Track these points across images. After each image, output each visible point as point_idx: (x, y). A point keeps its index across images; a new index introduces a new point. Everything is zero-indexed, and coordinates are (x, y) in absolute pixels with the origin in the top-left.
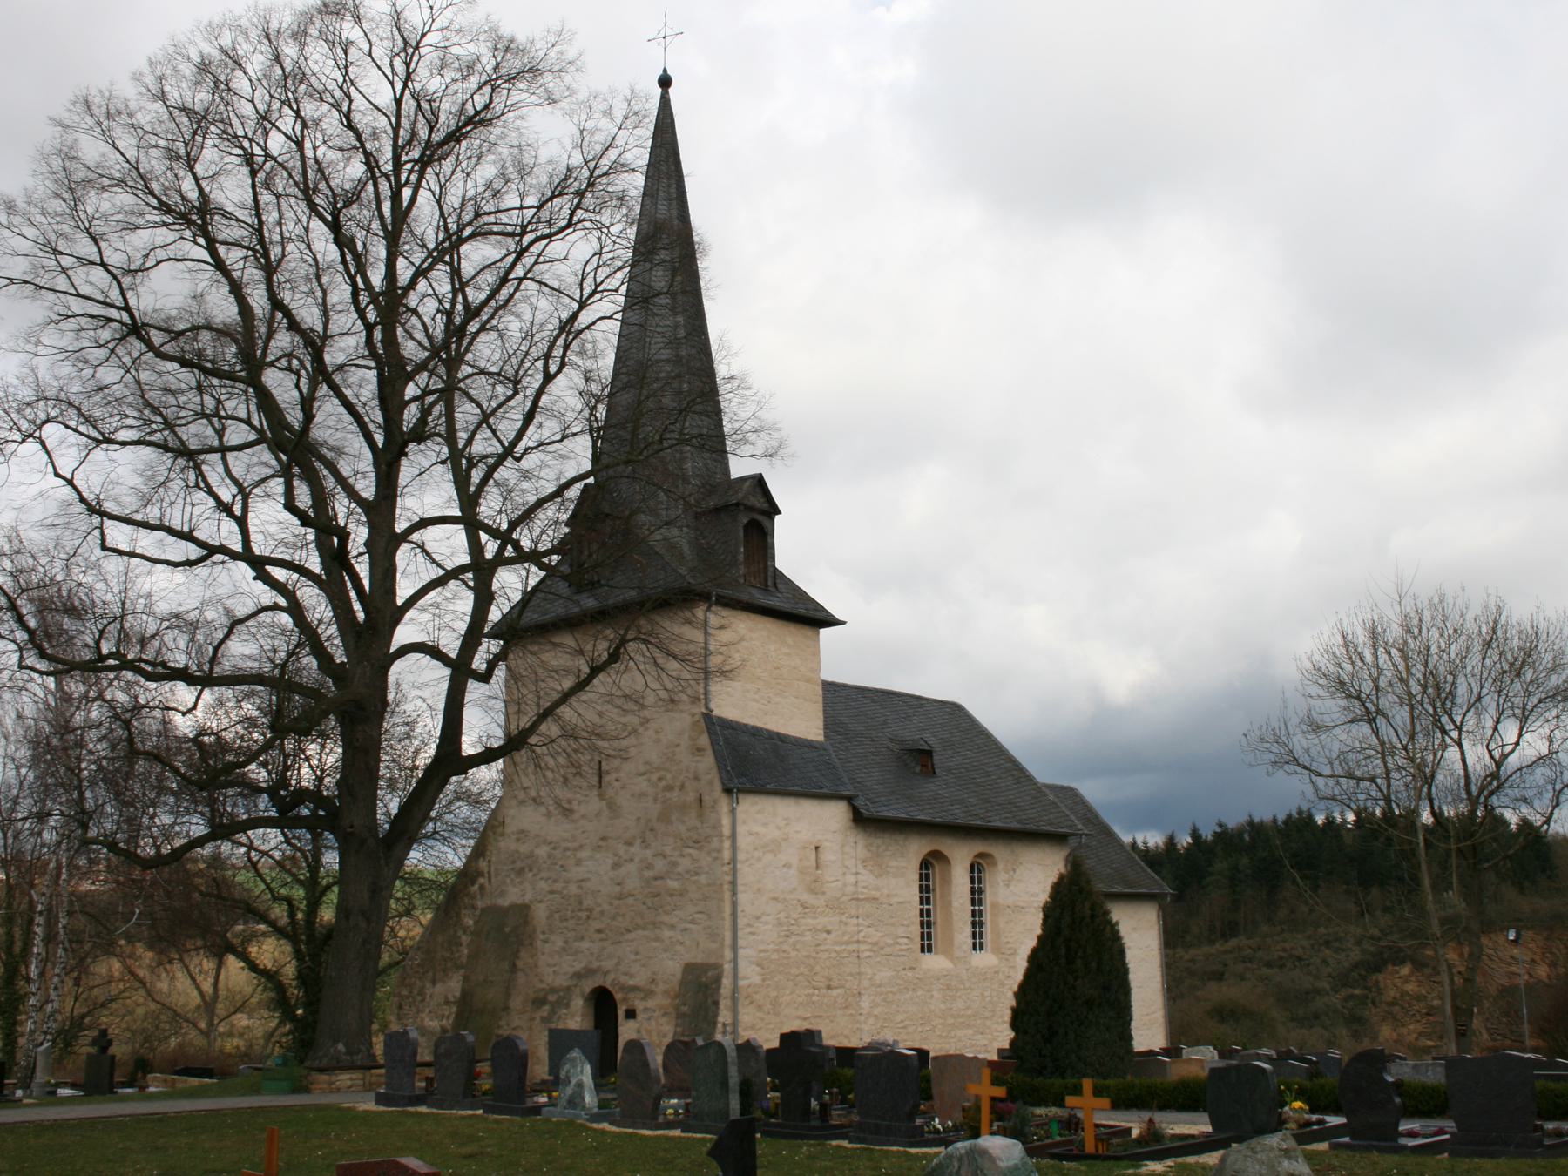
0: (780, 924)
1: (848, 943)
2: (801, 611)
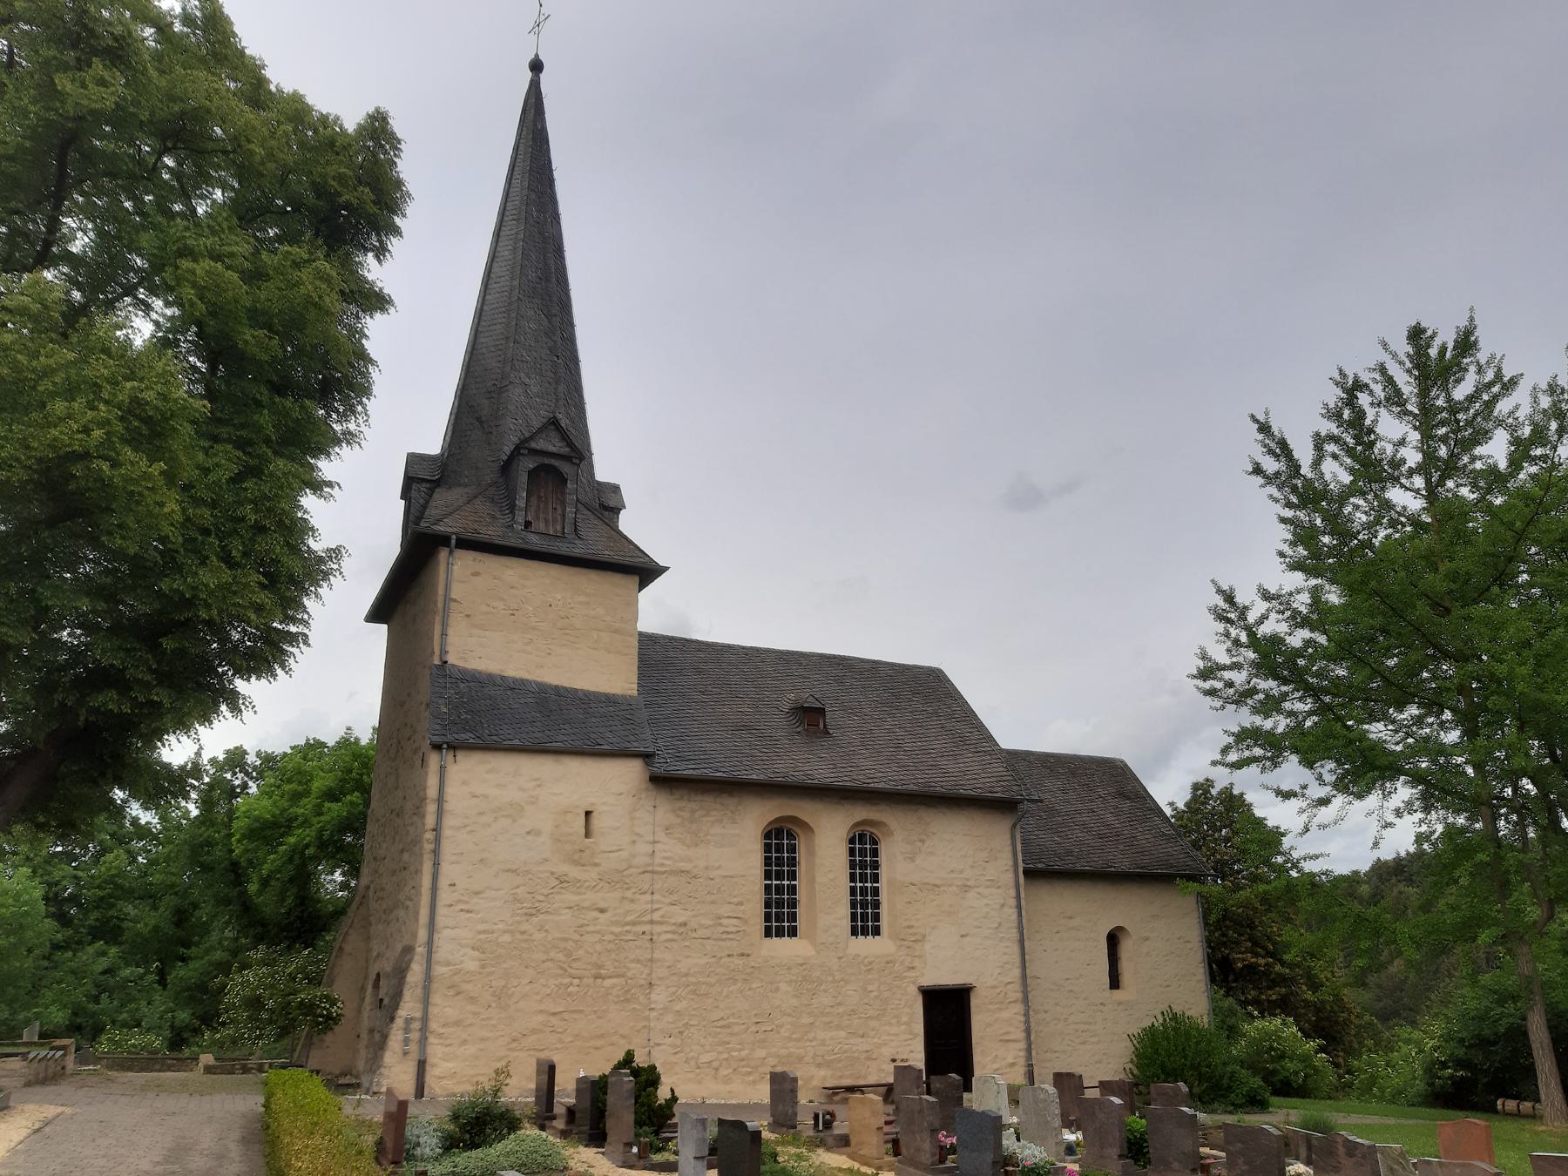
1: (634, 924)
2: (627, 560)
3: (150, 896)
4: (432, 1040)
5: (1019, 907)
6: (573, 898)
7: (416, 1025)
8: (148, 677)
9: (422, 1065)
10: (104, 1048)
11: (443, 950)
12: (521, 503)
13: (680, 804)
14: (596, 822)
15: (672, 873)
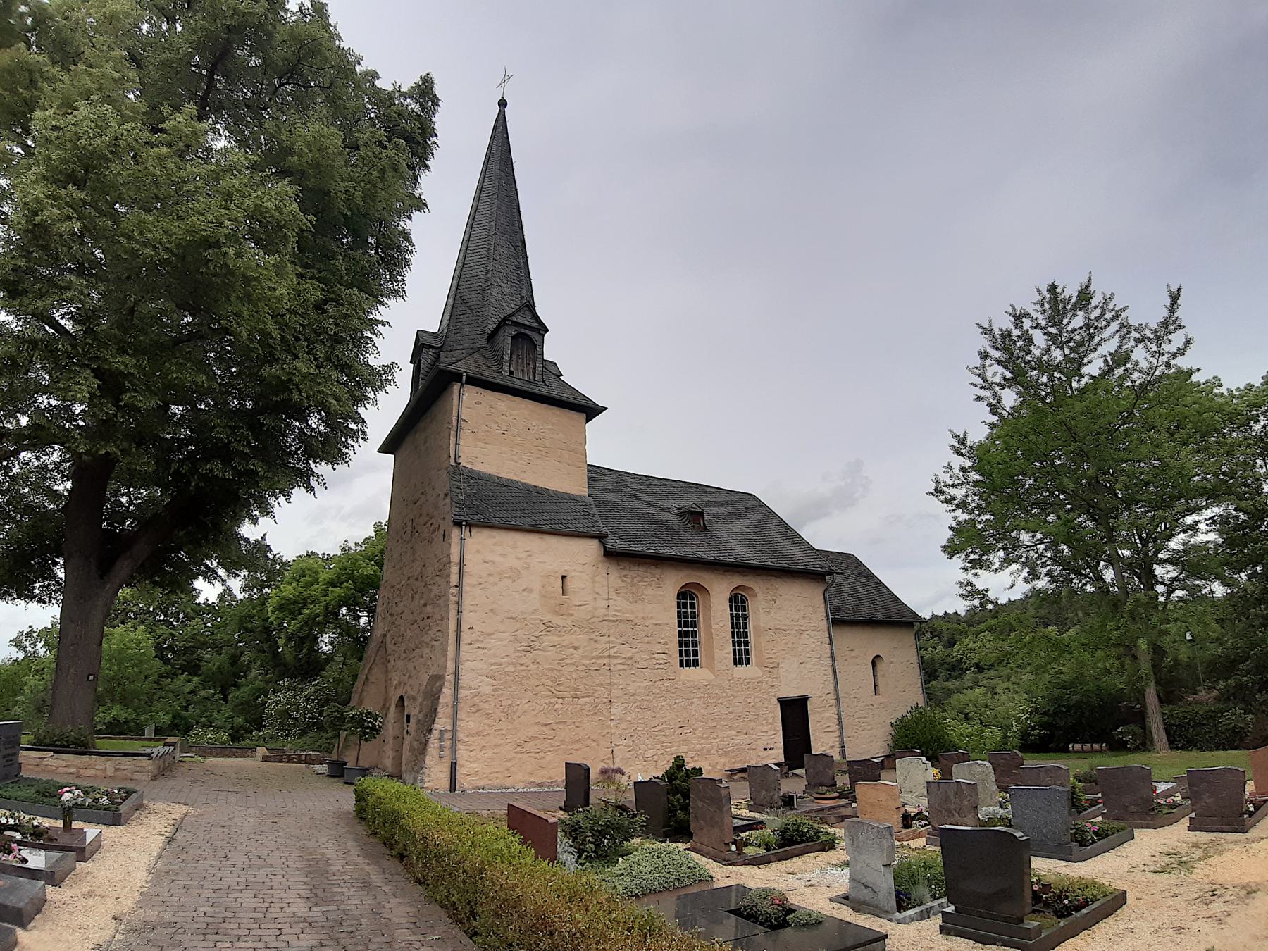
1: (597, 658)
3: (217, 648)
4: (460, 746)
5: (831, 643)
6: (556, 639)
7: (448, 735)
8: (247, 450)
9: (454, 766)
10: (193, 739)
11: (467, 678)
12: (507, 358)
13: (626, 572)
14: (570, 583)
15: (620, 621)
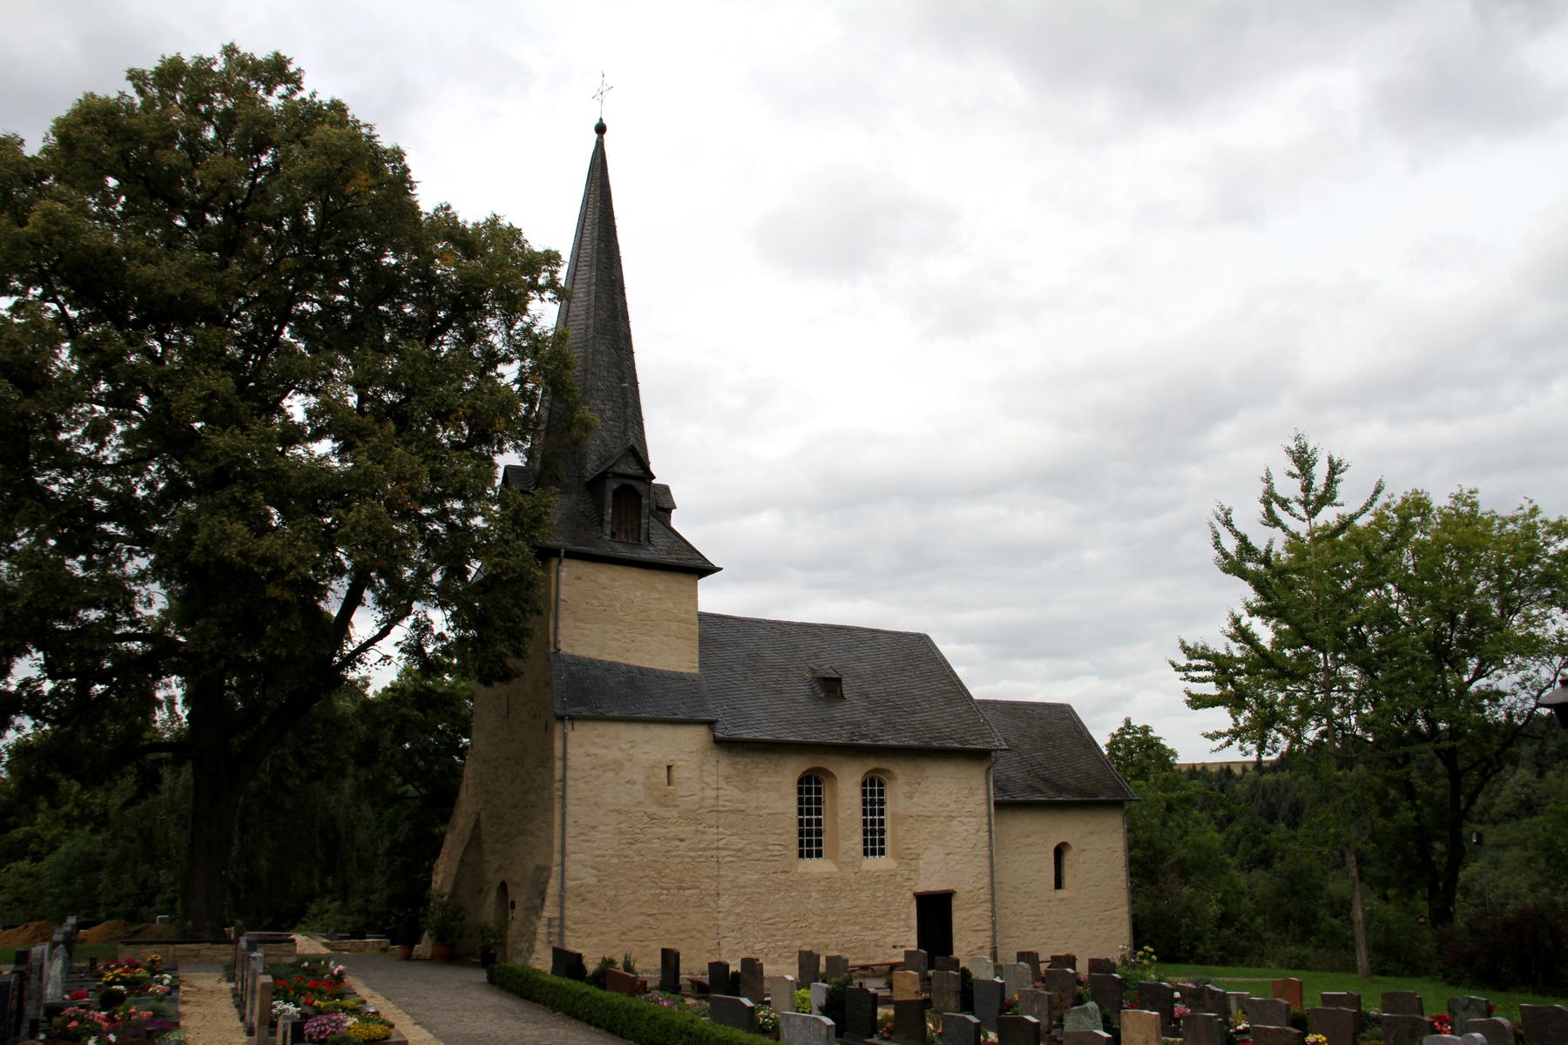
0: (621, 832)
1: (704, 849)
